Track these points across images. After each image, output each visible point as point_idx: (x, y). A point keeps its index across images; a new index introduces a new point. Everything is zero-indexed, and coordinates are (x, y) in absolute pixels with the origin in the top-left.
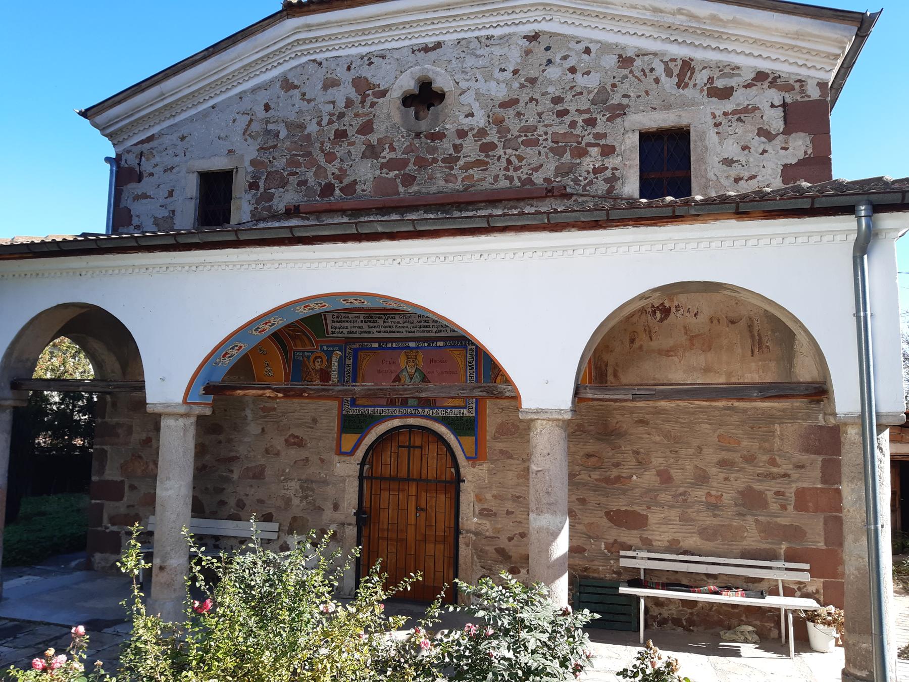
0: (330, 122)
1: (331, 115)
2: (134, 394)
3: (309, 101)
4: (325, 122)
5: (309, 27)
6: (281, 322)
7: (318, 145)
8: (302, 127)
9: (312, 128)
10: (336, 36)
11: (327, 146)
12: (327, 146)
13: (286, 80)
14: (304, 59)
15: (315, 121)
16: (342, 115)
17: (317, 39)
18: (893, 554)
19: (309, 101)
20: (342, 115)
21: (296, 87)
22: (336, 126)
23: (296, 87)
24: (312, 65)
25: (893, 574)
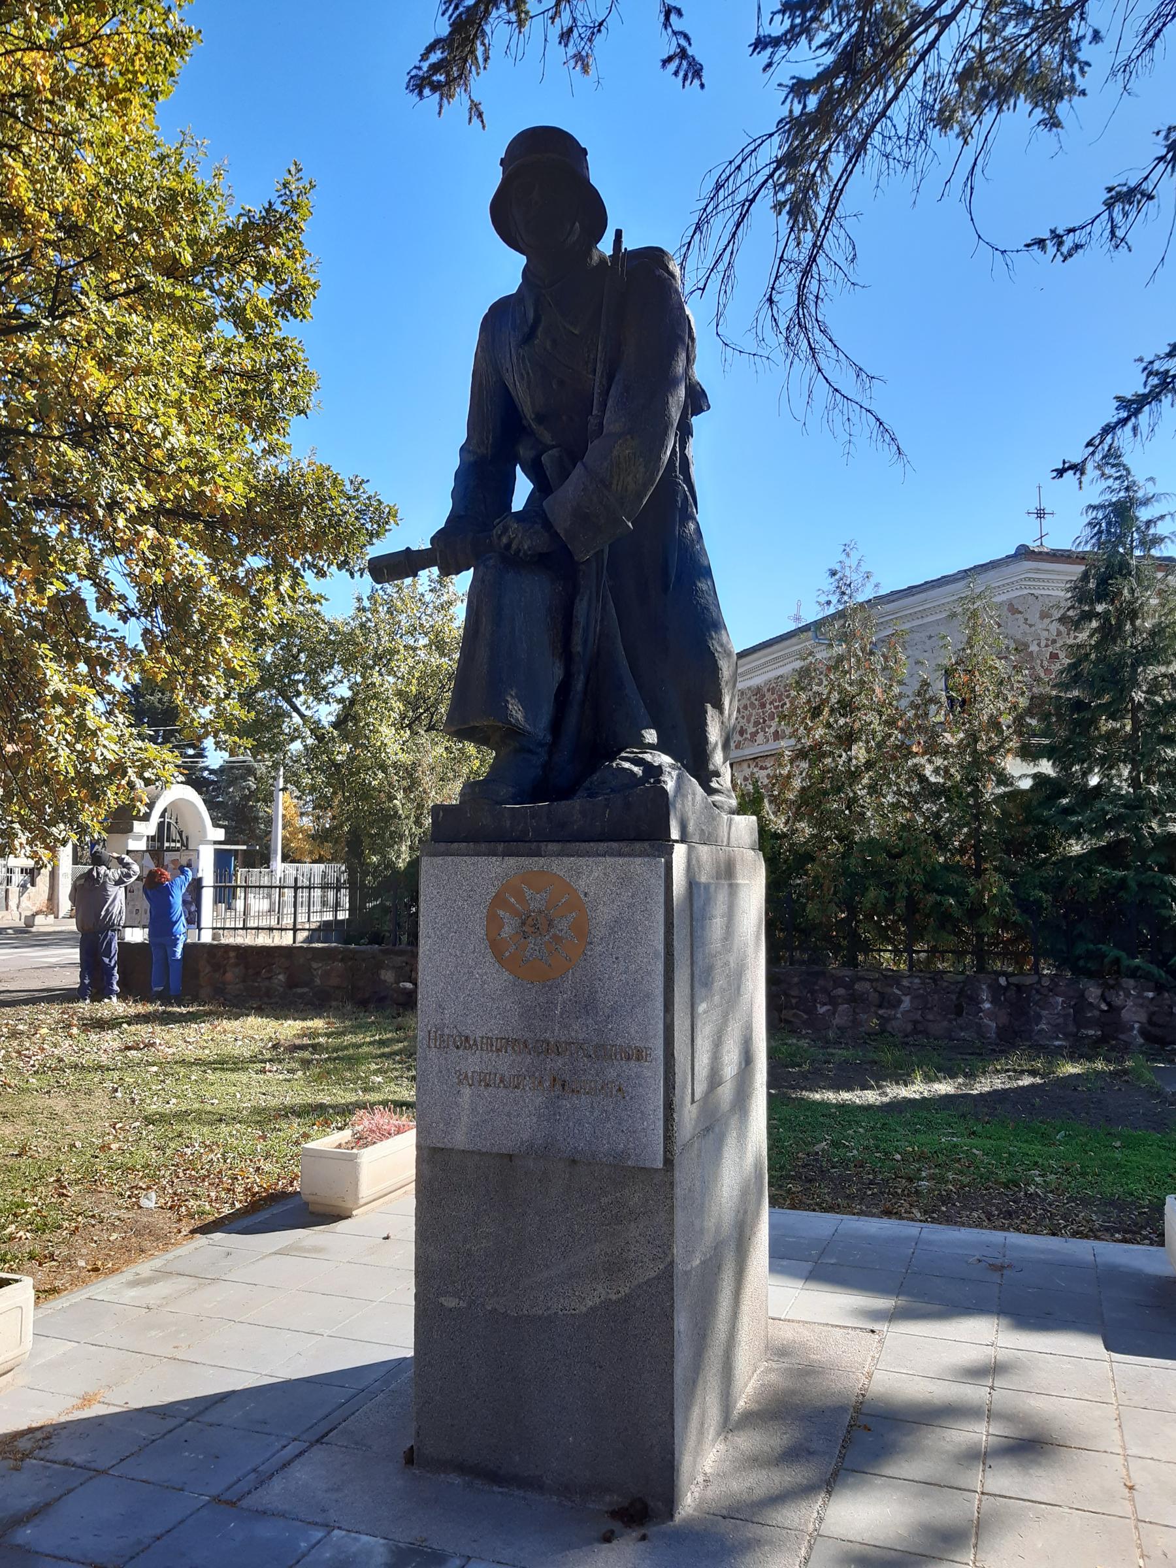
0: (1047, 646)
1: (1047, 639)
2: (582, 677)
3: (1031, 626)
4: (1043, 643)
5: (1038, 570)
6: (115, 276)
7: (1039, 662)
8: (1027, 645)
9: (1033, 648)
10: (1053, 581)
11: (1045, 663)
12: (1045, 663)
13: (1011, 605)
14: (1026, 592)
15: (1035, 642)
16: (1054, 641)
17: (1039, 579)
18: (771, 1257)
19: (1031, 626)
20: (1054, 641)
21: (1020, 612)
22: (1050, 649)
23: (1020, 612)
24: (1030, 597)
25: (703, 391)
